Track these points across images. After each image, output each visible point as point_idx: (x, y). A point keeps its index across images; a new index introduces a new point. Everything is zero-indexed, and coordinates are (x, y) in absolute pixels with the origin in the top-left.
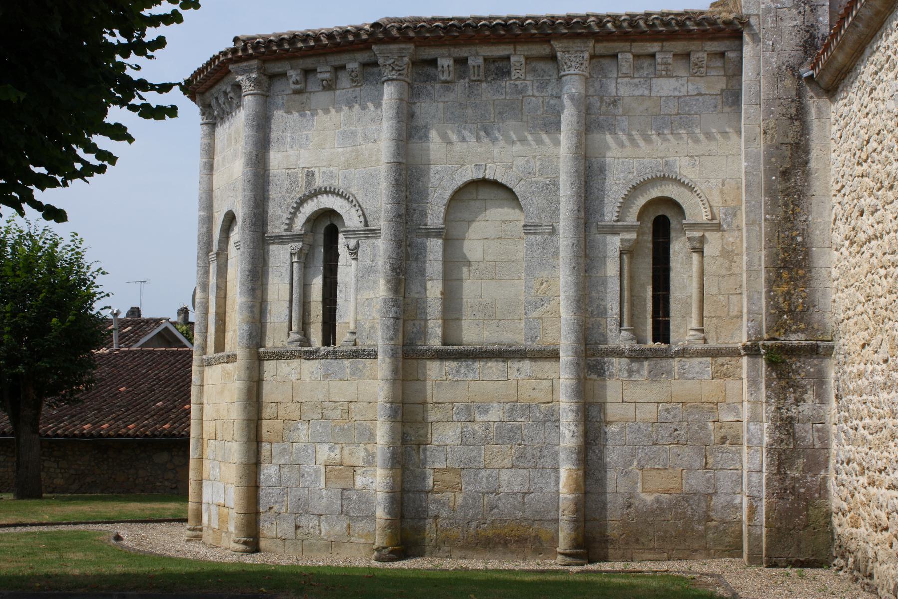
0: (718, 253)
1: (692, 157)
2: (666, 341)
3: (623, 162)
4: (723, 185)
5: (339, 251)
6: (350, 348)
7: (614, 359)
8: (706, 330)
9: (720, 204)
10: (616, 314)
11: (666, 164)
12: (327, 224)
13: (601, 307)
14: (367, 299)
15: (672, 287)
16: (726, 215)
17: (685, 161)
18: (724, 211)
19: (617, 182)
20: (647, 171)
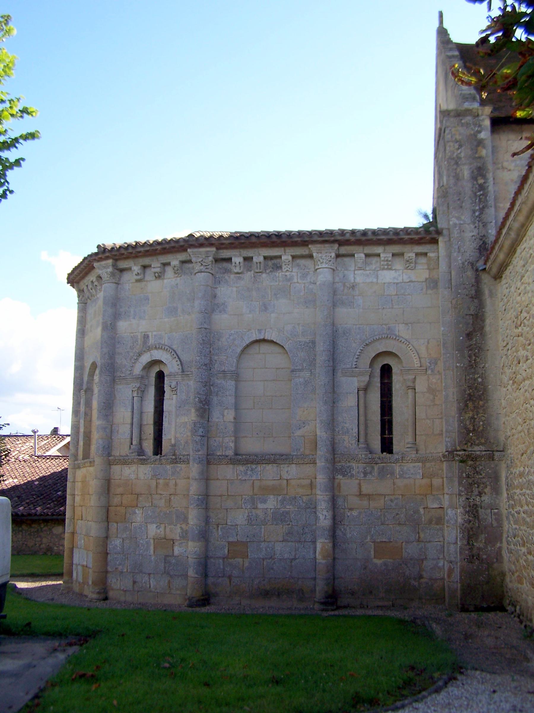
0: (425, 390)
1: (406, 324)
2: (390, 452)
3: (359, 328)
4: (428, 343)
5: (165, 389)
6: (171, 457)
7: (354, 464)
8: (417, 443)
9: (426, 356)
10: (356, 433)
11: (389, 328)
12: (157, 371)
13: (345, 428)
14: (183, 423)
15: (394, 414)
16: (430, 364)
17: (402, 327)
18: (429, 361)
19: (356, 341)
20: (376, 333)
